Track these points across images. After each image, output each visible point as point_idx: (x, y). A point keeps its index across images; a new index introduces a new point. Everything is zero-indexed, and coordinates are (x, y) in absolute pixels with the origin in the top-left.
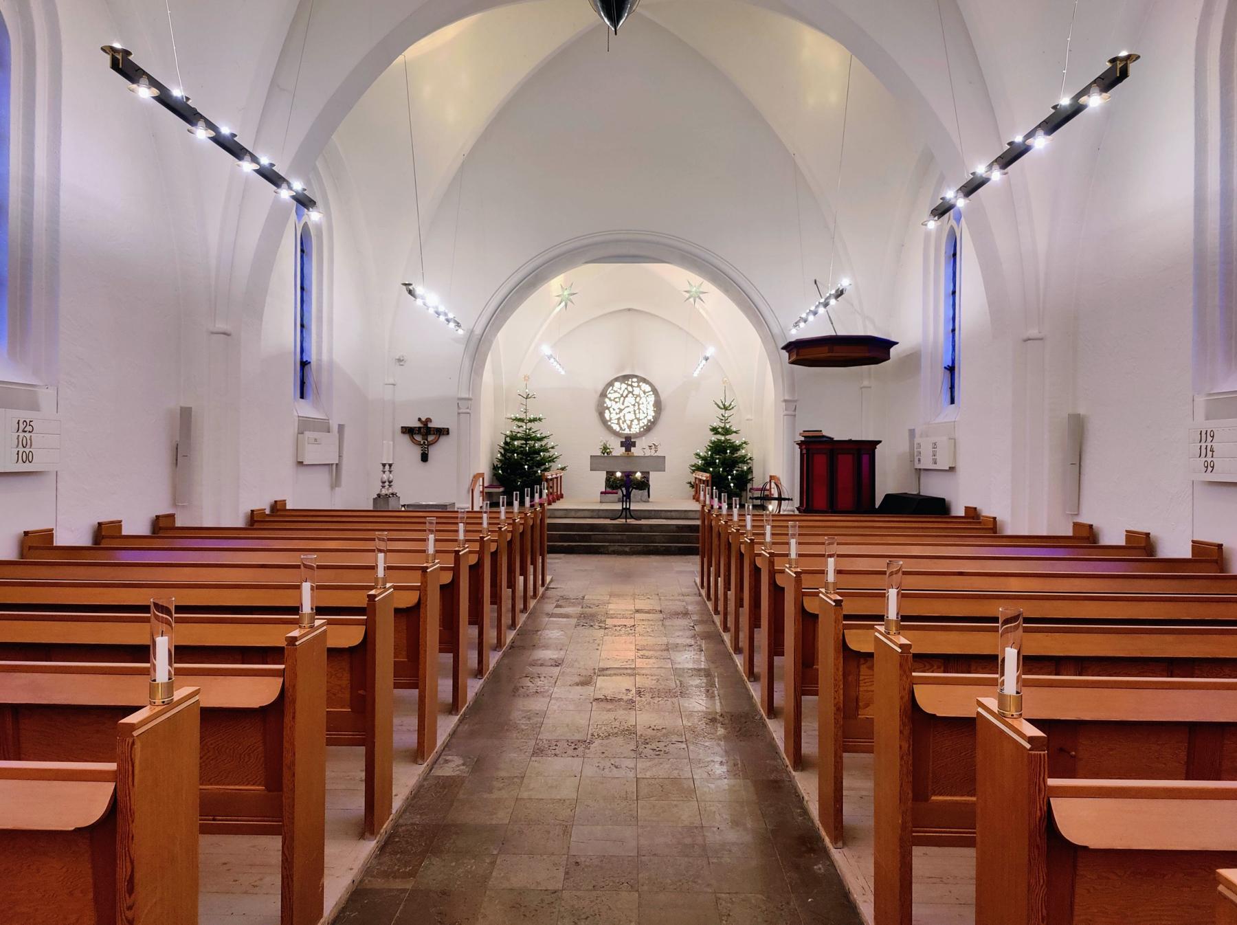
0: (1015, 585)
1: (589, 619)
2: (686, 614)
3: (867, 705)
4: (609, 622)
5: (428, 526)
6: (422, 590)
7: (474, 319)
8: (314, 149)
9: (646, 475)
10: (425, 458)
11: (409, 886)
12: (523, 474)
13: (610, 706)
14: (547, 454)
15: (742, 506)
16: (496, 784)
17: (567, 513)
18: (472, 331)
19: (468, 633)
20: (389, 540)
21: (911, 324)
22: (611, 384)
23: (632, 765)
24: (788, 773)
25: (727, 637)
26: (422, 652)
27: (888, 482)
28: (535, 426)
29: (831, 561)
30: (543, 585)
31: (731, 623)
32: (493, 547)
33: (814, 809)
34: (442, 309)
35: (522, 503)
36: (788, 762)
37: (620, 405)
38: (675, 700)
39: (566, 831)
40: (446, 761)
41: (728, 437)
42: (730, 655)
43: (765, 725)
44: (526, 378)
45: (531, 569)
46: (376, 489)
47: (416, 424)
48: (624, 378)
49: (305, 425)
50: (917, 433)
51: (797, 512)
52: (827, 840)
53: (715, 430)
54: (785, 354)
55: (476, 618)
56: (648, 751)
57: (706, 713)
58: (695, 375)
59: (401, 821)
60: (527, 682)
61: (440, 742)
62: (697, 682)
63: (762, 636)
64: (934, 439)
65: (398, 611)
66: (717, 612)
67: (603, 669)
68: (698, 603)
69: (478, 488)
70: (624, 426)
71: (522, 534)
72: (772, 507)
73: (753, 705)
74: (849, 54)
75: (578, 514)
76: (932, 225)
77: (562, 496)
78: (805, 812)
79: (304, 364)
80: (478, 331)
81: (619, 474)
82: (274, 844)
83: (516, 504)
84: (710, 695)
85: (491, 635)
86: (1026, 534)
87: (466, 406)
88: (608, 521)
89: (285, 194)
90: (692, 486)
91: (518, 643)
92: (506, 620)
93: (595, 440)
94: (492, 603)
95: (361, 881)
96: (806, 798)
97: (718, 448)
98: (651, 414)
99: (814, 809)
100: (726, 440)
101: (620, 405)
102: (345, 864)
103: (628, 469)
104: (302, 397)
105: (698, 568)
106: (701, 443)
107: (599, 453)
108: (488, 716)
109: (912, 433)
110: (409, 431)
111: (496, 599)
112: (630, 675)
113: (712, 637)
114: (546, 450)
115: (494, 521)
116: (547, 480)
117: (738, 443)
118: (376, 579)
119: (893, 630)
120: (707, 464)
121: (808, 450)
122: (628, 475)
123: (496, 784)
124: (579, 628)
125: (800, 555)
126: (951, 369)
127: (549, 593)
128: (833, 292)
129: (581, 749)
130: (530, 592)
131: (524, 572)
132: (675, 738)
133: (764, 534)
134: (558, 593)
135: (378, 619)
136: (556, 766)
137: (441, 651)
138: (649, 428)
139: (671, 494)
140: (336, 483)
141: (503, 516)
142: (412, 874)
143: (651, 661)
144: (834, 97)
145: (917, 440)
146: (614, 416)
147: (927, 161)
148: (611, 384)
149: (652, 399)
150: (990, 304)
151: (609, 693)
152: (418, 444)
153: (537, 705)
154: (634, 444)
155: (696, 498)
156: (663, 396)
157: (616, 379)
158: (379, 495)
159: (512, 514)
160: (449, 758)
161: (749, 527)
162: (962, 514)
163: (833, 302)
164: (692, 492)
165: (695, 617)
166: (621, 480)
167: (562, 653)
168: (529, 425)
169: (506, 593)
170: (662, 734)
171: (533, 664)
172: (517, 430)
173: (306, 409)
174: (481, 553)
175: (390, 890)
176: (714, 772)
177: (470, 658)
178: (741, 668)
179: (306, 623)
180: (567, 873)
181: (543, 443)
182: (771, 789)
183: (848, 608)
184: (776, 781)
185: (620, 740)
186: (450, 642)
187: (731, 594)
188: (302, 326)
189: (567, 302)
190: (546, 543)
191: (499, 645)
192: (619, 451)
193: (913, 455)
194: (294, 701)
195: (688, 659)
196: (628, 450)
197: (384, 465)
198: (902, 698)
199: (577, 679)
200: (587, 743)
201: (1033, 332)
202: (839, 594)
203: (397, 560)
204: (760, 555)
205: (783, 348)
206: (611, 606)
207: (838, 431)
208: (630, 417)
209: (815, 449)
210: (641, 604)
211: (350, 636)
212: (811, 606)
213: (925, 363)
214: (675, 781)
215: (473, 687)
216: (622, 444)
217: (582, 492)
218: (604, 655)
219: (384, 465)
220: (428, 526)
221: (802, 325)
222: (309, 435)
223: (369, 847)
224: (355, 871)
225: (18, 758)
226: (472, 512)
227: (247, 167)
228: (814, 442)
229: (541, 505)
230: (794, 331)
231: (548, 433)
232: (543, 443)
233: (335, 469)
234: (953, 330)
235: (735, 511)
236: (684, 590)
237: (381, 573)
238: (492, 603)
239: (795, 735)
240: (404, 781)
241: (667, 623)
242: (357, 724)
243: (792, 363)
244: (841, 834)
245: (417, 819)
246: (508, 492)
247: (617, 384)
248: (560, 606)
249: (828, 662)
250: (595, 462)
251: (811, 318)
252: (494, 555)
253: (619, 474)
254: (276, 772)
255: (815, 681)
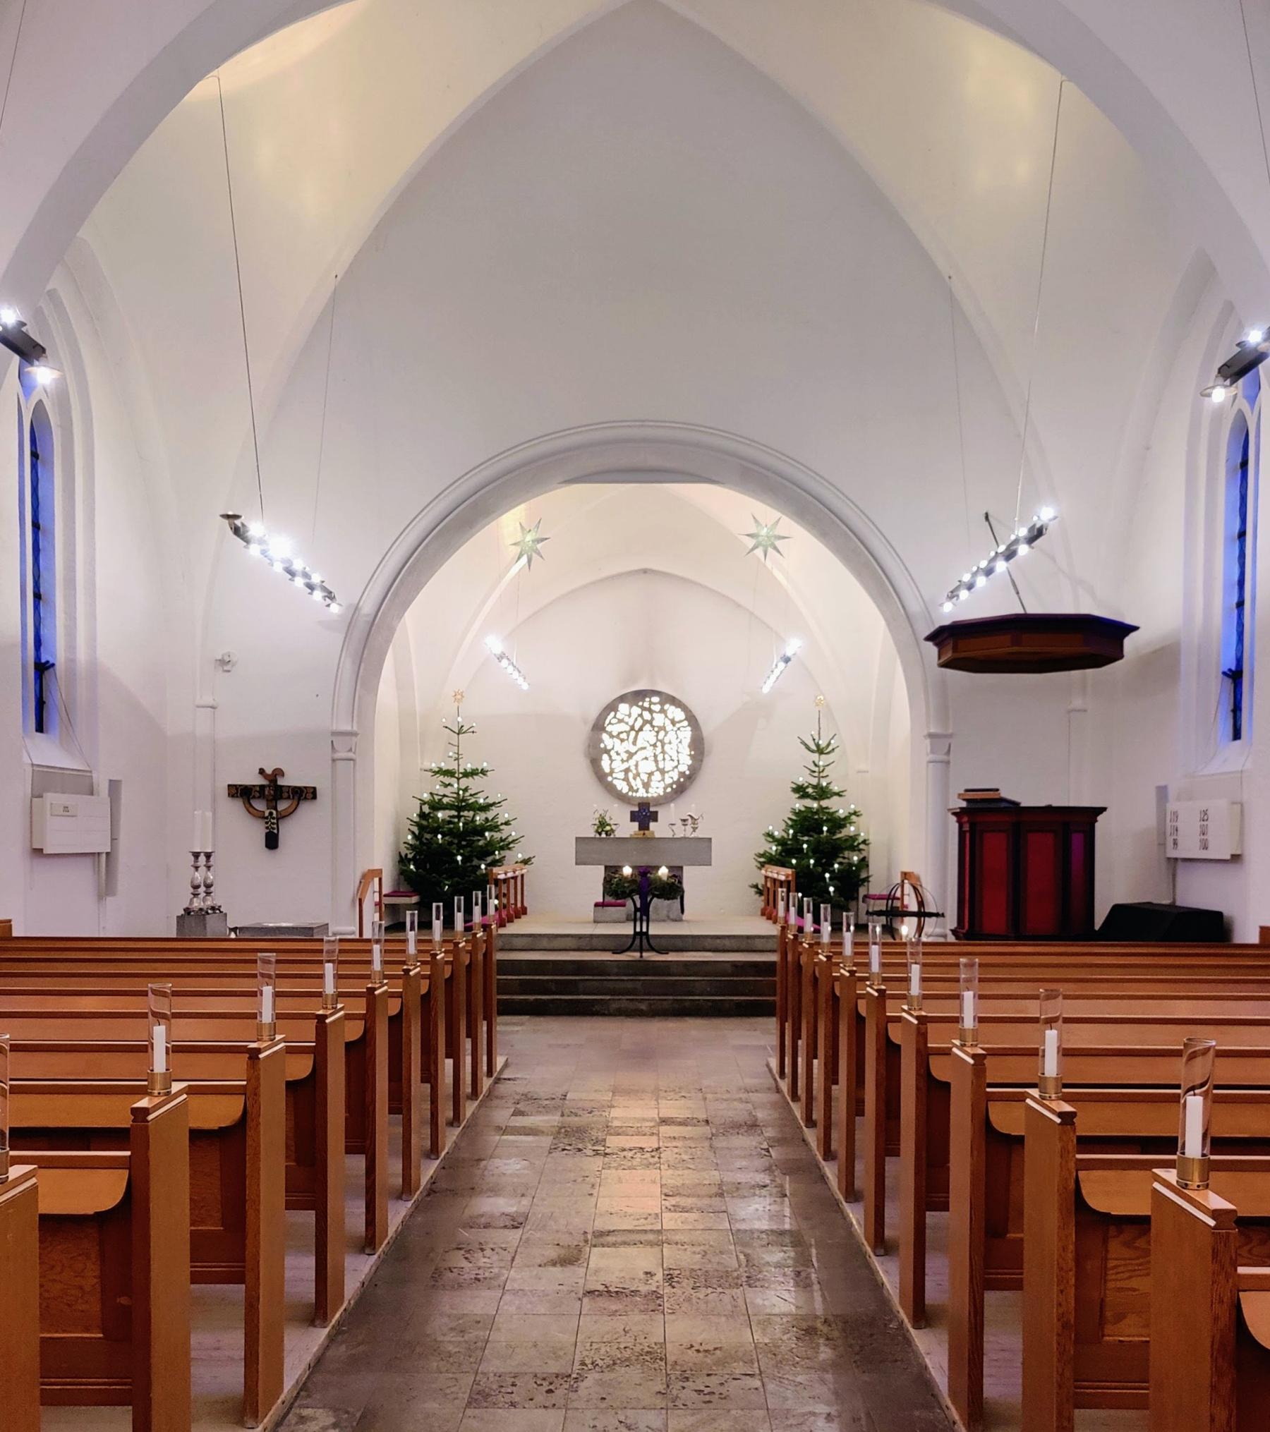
1: (575, 1136)
2: (753, 1126)
4: (613, 1142)
5: (259, 968)
6: (250, 1093)
7: (359, 584)
9: (676, 872)
10: (272, 842)
12: (455, 871)
14: (497, 835)
15: (861, 928)
17: (534, 942)
18: (357, 608)
19: (345, 1168)
21: (1163, 589)
22: (612, 707)
25: (831, 1171)
27: (1118, 880)
28: (473, 784)
29: (1051, 1035)
30: (490, 1073)
32: (394, 1007)
34: (298, 565)
35: (449, 923)
36: (955, 1415)
40: (302, 1419)
41: (824, 803)
42: (837, 1203)
43: (908, 1341)
44: (459, 697)
45: (467, 1044)
46: (182, 900)
48: (637, 697)
50: (1172, 793)
51: (951, 939)
53: (800, 791)
54: (932, 650)
55: (361, 1139)
56: (688, 1395)
57: (796, 1317)
58: (766, 689)
60: (458, 1259)
61: (289, 1383)
62: (775, 1255)
63: (902, 1170)
64: (1203, 805)
65: (196, 1135)
66: (810, 1123)
67: (602, 1234)
68: (774, 1105)
69: (371, 898)
70: (637, 784)
71: (449, 981)
72: (907, 929)
73: (884, 1302)
74: (1058, 77)
75: (556, 944)
77: (524, 911)
79: (42, 668)
80: (368, 608)
81: (627, 871)
83: (437, 925)
84: (802, 1282)
85: (391, 1169)
87: (346, 746)
90: (760, 893)
92: (420, 1139)
93: (585, 810)
97: (806, 823)
98: (686, 762)
100: (822, 809)
103: (644, 861)
104: (40, 728)
105: (774, 1040)
106: (777, 816)
109: (1162, 792)
110: (241, 793)
111: (400, 1103)
112: (651, 1244)
113: (802, 1170)
114: (495, 828)
115: (394, 957)
116: (497, 882)
117: (842, 813)
118: (151, 1076)
119: (1196, 1181)
120: (786, 852)
121: (972, 825)
122: (644, 872)
124: (557, 1154)
125: (981, 1020)
126: (1235, 676)
127: (502, 1088)
128: (1023, 532)
129: (560, 1392)
130: (467, 1088)
132: (739, 1368)
134: (519, 1088)
135: (153, 1154)
138: (681, 788)
139: (722, 904)
140: (106, 887)
141: (412, 949)
143: (692, 1216)
145: (1171, 806)
146: (619, 766)
148: (612, 707)
149: (686, 734)
151: (613, 1280)
153: (478, 1303)
154: (654, 817)
155: (768, 913)
156: (706, 730)
157: (622, 699)
159: (433, 942)
160: (305, 1412)
161: (875, 968)
162: (1254, 938)
163: (1023, 549)
164: (760, 902)
165: (770, 1133)
166: (632, 881)
167: (526, 1201)
168: (465, 782)
169: (419, 1090)
170: (716, 1359)
171: (470, 1225)
172: (442, 791)
173: (47, 752)
174: (369, 1019)
177: (350, 1214)
178: (858, 1229)
181: (490, 815)
183: (1089, 1124)
185: (634, 1373)
186: (308, 1188)
188: (37, 596)
189: (531, 554)
190: (496, 997)
191: (407, 1188)
192: (626, 828)
193: (1164, 832)
195: (758, 1212)
196: (644, 827)
197: (196, 855)
198: (1216, 1319)
199: (552, 1253)
200: (570, 1379)
202: (1067, 1099)
206: (615, 1113)
209: (987, 826)
212: (1005, 1120)
213: (1188, 664)
215: (357, 1271)
216: (634, 817)
217: (562, 902)
218: (604, 1205)
219: (196, 855)
220: (259, 968)
221: (964, 594)
222: (53, 799)
223: (322, 1334)
225: (89, 1150)
228: (990, 810)
229: (486, 927)
230: (948, 607)
231: (499, 797)
232: (490, 815)
233: (104, 865)
234: (1240, 604)
235: (848, 937)
236: (750, 1082)
237: (159, 1063)
239: (970, 1361)
241: (720, 1143)
246: (424, 907)
247: (624, 708)
248: (522, 1113)
249: (1042, 1228)
250: (585, 851)
251: (981, 581)
252: (396, 1022)
253: (627, 871)
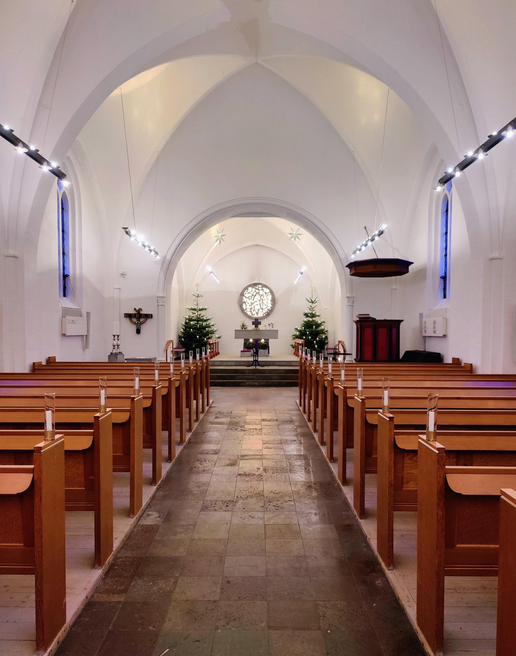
0: (491, 404)
1: (235, 425)
2: (291, 421)
3: (408, 482)
4: (247, 427)
5: (134, 372)
7: (166, 249)
8: (67, 142)
9: (267, 341)
10: (138, 331)
11: (122, 599)
12: (196, 341)
13: (247, 479)
14: (210, 329)
15: (326, 358)
16: (179, 530)
17: (222, 363)
18: (165, 257)
19: (162, 435)
20: (108, 380)
21: (421, 252)
22: (246, 288)
23: (261, 516)
24: (357, 521)
25: (316, 436)
26: (132, 449)
27: (407, 343)
28: (202, 313)
29: (386, 393)
30: (208, 405)
31: (318, 427)
32: (177, 384)
33: (374, 543)
34: (146, 244)
35: (194, 357)
37: (251, 301)
38: (287, 474)
39: (222, 560)
40: (148, 515)
41: (314, 319)
43: (341, 490)
44: (198, 285)
45: (200, 396)
46: (110, 350)
47: (133, 312)
48: (254, 285)
49: (66, 312)
51: (354, 362)
52: (383, 564)
53: (306, 315)
54: (348, 270)
55: (167, 426)
56: (271, 507)
57: (305, 482)
58: (295, 283)
59: (119, 555)
60: (198, 464)
61: (144, 504)
63: (339, 435)
64: (434, 319)
65: (115, 425)
66: (310, 420)
67: (243, 456)
69: (170, 349)
70: (254, 313)
72: (340, 359)
73: (333, 477)
74: (387, 87)
75: (229, 364)
76: (439, 189)
77: (218, 353)
78: (368, 546)
79: (65, 277)
80: (169, 257)
81: (251, 340)
82: (30, 580)
83: (191, 358)
84: (307, 471)
85: (176, 435)
86: (501, 373)
87: (162, 301)
88: (245, 368)
89: (45, 169)
90: (293, 347)
91: (193, 440)
92: (186, 426)
93: (237, 321)
94: (187, 407)
95: (92, 596)
96: (369, 536)
97: (308, 325)
98: (270, 306)
99: (374, 543)
100: (313, 321)
101: (251, 301)
102: (80, 586)
103: (256, 337)
104: (65, 295)
105: (298, 394)
106: (299, 323)
107: (240, 329)
108: (174, 486)
109: (421, 315)
110: (128, 316)
111: (179, 414)
112: (259, 459)
113: (307, 435)
114: (209, 327)
116: (210, 344)
117: (319, 322)
118: (100, 406)
119: (432, 438)
120: (302, 334)
122: (257, 341)
123: (179, 530)
125: (364, 388)
126: (444, 278)
127: (212, 410)
129: (230, 506)
130: (200, 410)
131: (196, 398)
132: (287, 499)
133: (340, 375)
135: (101, 431)
136: (216, 516)
137: (144, 447)
138: (268, 314)
139: (281, 351)
140: (86, 346)
141: (183, 365)
142: (125, 591)
144: (377, 117)
145: (424, 320)
146: (248, 307)
147: (434, 151)
148: (246, 288)
149: (270, 297)
150: (471, 238)
152: (134, 323)
153: (204, 478)
154: (260, 323)
155: (296, 354)
156: (277, 295)
157: (249, 286)
158: (112, 354)
159: (189, 364)
160: (149, 513)
161: (330, 371)
162: (450, 362)
163: (377, 238)
164: (293, 350)
166: (253, 343)
167: (219, 446)
168: (199, 312)
169: (185, 410)
171: (201, 453)
172: (192, 315)
173: (67, 303)
174: (169, 388)
175: (110, 602)
176: (310, 520)
177: (164, 450)
179: (49, 438)
180: (222, 589)
181: (208, 323)
182: (346, 530)
184: (348, 525)
185: (254, 500)
186: (150, 441)
187: (319, 410)
188: (64, 254)
189: (220, 240)
191: (181, 442)
192: (251, 327)
193: (422, 328)
194: (40, 489)
195: (294, 449)
196: (256, 326)
197: (114, 336)
198: (439, 482)
199: (228, 462)
200: (234, 502)
201: (496, 255)
202: (391, 413)
203: (113, 392)
204: (337, 388)
205: (347, 266)
206: (247, 417)
207: (379, 315)
208: (258, 307)
209: (366, 326)
210: (265, 416)
211: (82, 442)
212: (372, 419)
213: (429, 274)
214: (288, 526)
215: (165, 468)
216: (253, 323)
217: (230, 350)
218: (244, 447)
219: (114, 336)
220: (134, 372)
221: (358, 252)
223: (98, 573)
224: (89, 589)
226: (167, 363)
227: (21, 150)
229: (206, 358)
230: (353, 257)
231: (210, 317)
232: (208, 323)
233: (85, 339)
234: (446, 255)
235: (321, 361)
236: (290, 407)
237: (103, 402)
238: (187, 407)
239: (360, 496)
240: (121, 528)
241: (281, 427)
242: (88, 496)
243: (351, 275)
244: (392, 561)
245: (129, 554)
246: (187, 352)
247: (250, 289)
248: (218, 418)
249: (383, 454)
250: (238, 334)
251: (363, 248)
252: (178, 389)
253: (251, 340)
254: (30, 534)
255: (375, 464)
